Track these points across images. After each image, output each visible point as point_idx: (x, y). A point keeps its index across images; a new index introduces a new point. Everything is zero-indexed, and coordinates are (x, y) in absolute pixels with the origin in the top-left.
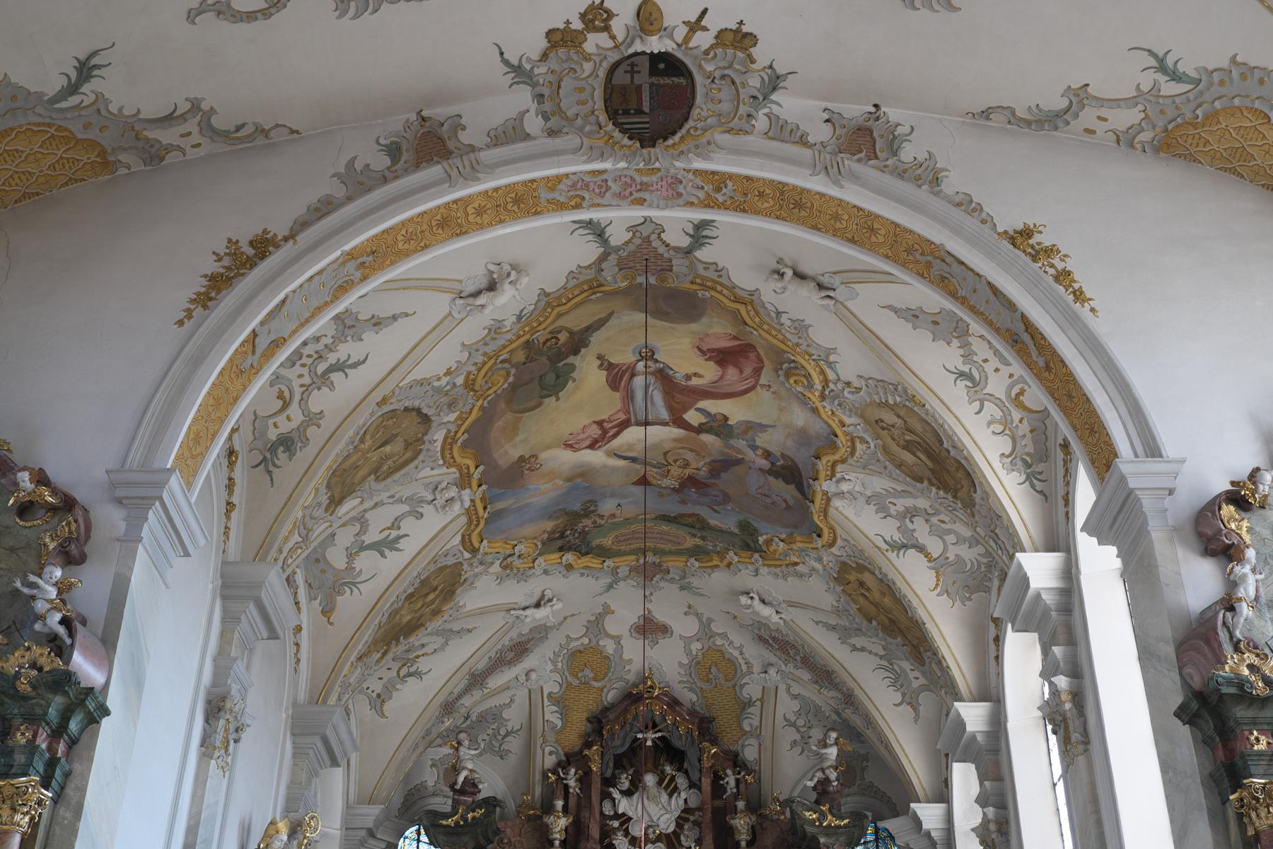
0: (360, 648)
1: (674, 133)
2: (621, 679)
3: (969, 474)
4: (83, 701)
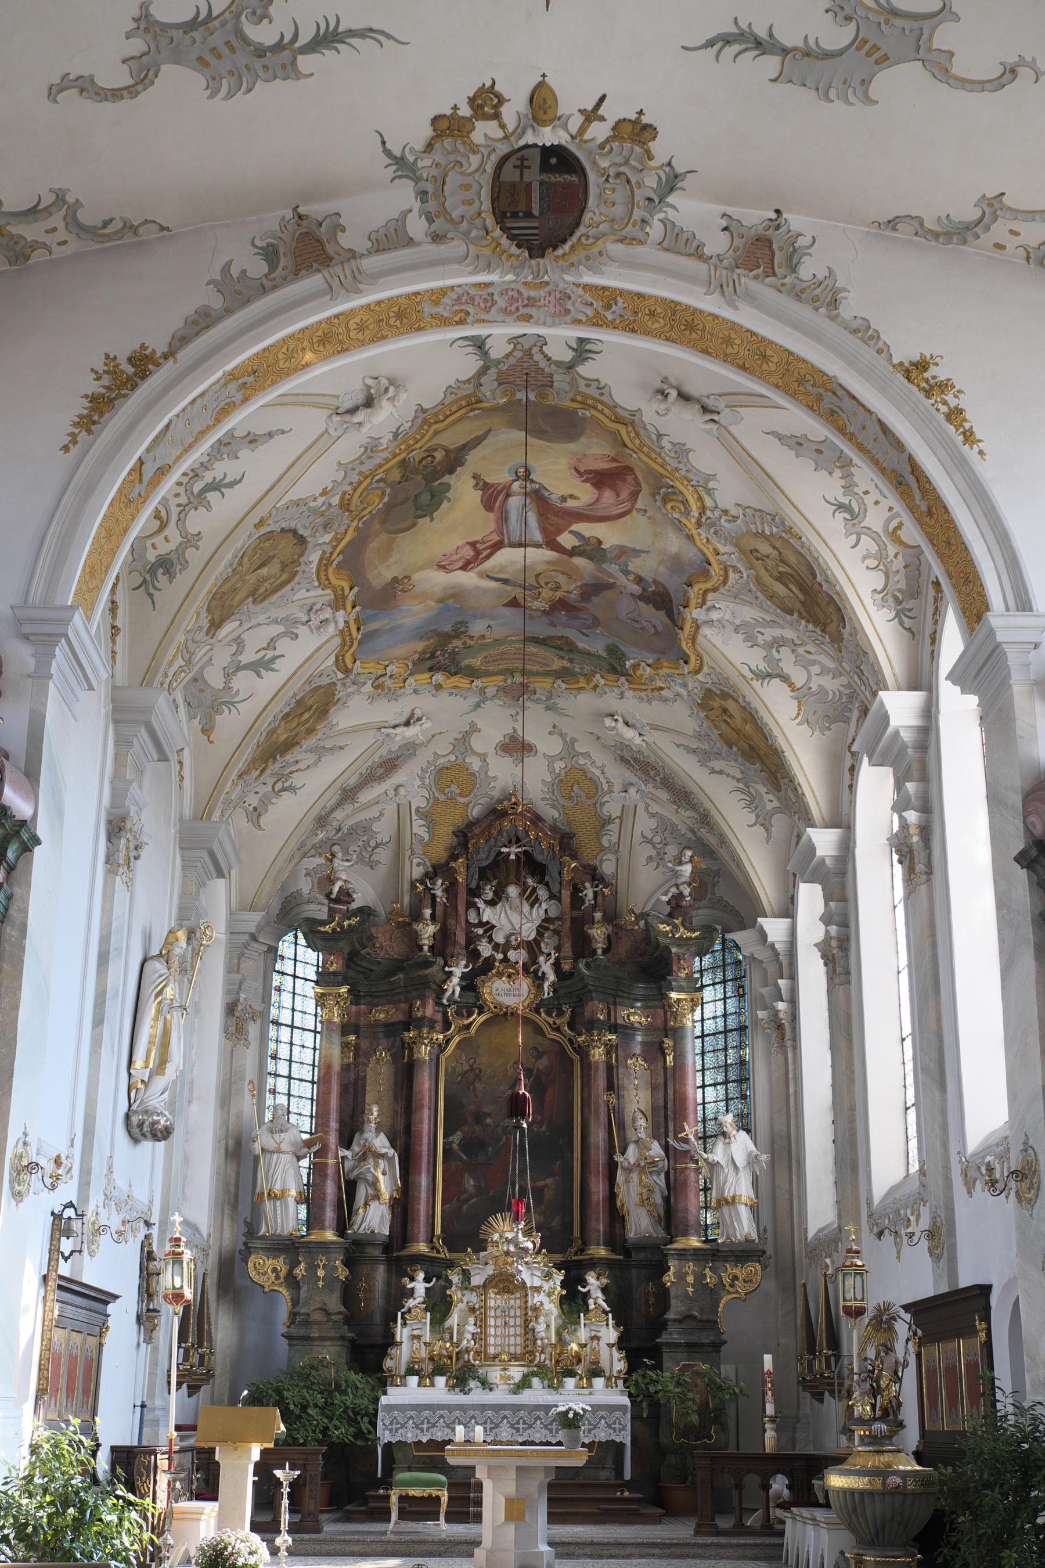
0: (240, 766)
1: (564, 241)
2: (486, 795)
3: (839, 609)
4: (18, 833)
